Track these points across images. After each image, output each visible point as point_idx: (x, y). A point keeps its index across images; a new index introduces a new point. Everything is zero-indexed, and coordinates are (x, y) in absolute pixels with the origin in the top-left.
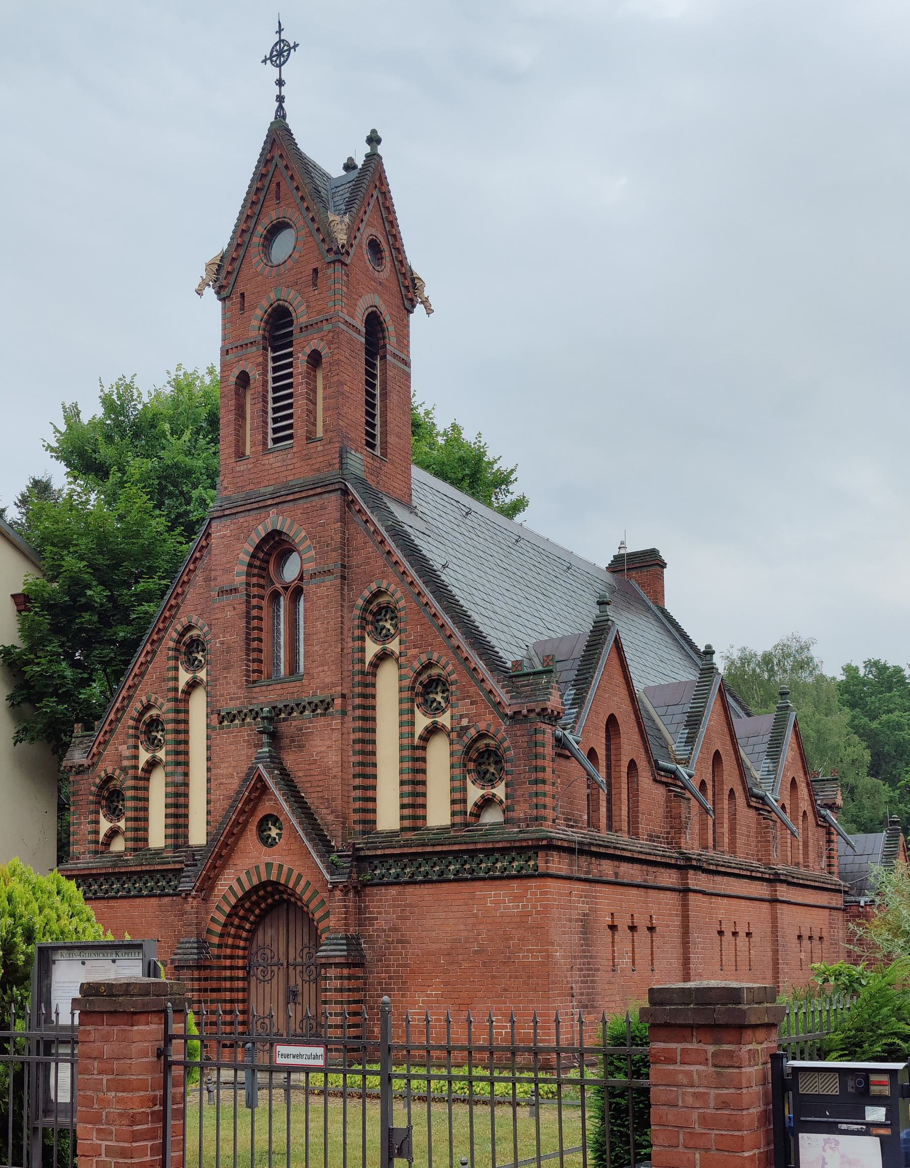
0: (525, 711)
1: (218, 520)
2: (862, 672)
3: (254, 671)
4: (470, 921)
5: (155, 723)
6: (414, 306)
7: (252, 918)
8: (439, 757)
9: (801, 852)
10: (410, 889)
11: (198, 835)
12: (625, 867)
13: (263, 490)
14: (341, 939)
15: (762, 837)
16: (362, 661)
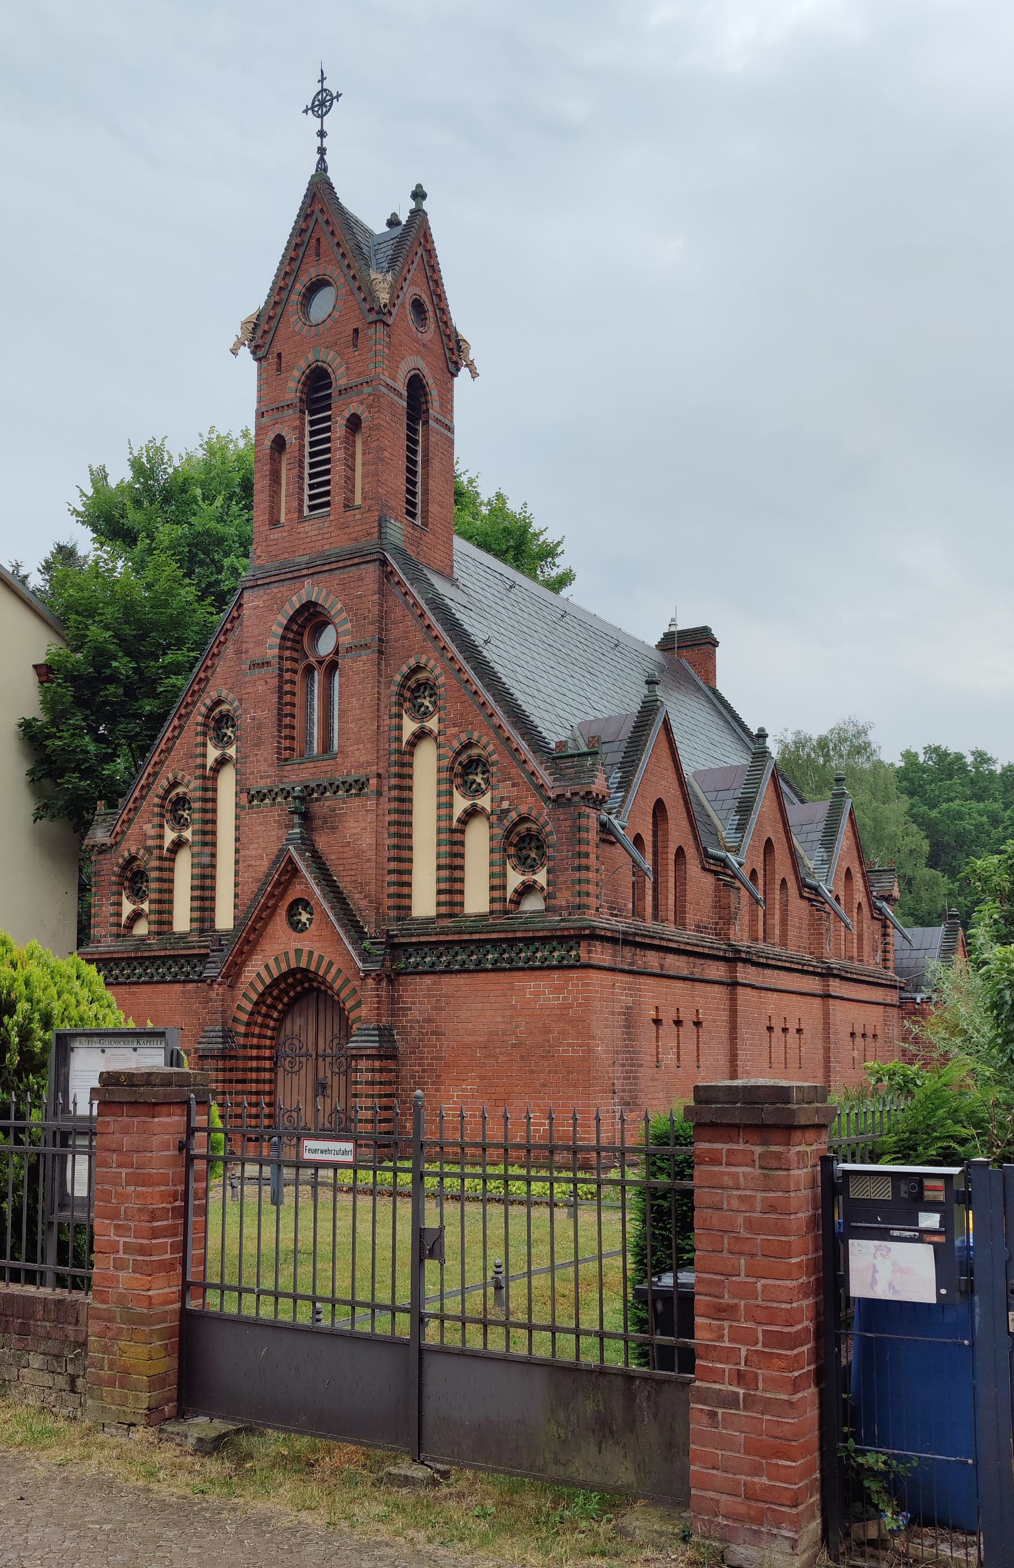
0: (568, 795)
1: (250, 590)
2: (921, 759)
3: (286, 749)
4: (508, 1013)
5: (182, 801)
6: (458, 370)
7: (280, 1007)
8: (478, 840)
9: (855, 945)
10: (446, 979)
11: (225, 919)
12: (670, 959)
13: (297, 560)
14: (373, 1029)
15: (814, 929)
16: (399, 739)
